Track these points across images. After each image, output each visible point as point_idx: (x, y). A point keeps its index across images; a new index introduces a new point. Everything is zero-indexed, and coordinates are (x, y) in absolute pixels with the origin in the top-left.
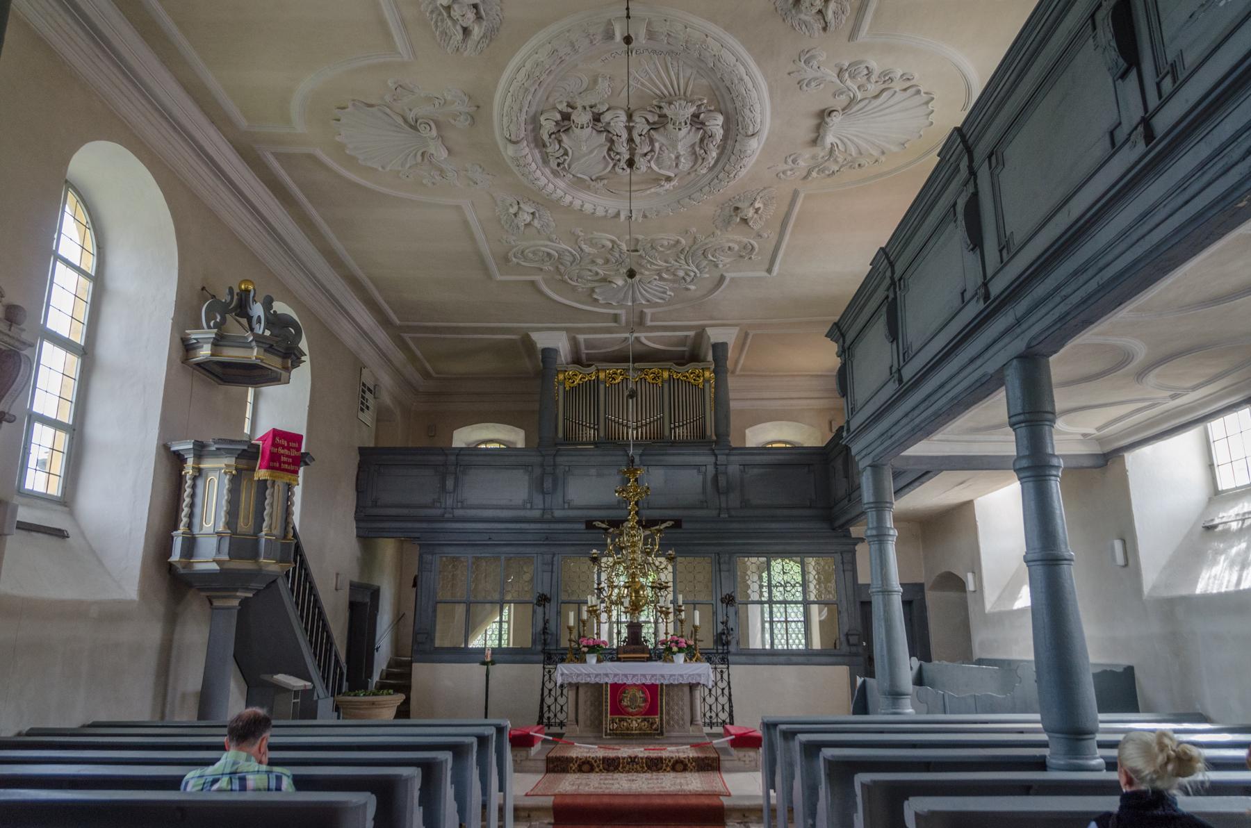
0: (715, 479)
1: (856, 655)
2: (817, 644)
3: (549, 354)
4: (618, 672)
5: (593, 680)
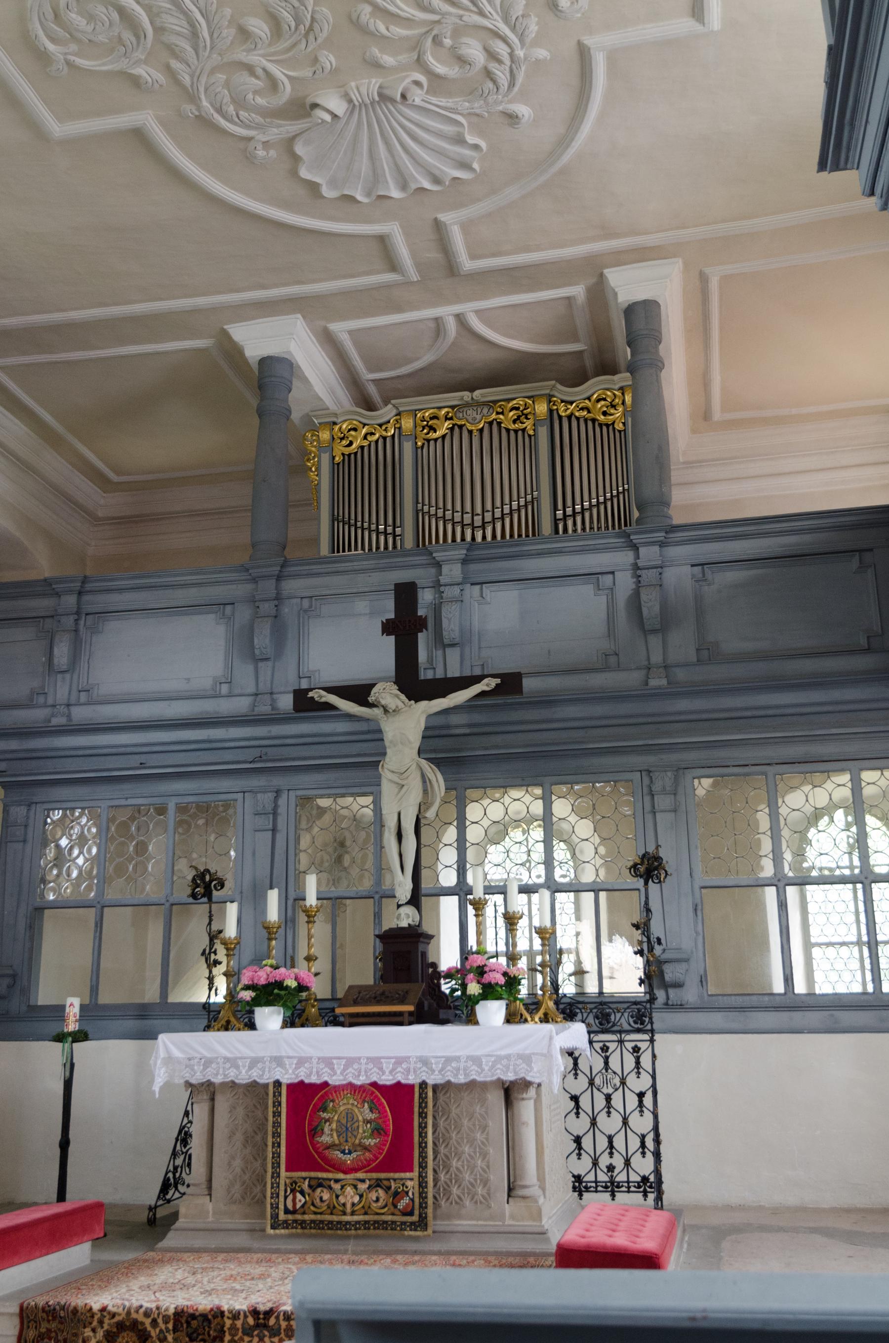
0: (635, 602)
5: (243, 1076)
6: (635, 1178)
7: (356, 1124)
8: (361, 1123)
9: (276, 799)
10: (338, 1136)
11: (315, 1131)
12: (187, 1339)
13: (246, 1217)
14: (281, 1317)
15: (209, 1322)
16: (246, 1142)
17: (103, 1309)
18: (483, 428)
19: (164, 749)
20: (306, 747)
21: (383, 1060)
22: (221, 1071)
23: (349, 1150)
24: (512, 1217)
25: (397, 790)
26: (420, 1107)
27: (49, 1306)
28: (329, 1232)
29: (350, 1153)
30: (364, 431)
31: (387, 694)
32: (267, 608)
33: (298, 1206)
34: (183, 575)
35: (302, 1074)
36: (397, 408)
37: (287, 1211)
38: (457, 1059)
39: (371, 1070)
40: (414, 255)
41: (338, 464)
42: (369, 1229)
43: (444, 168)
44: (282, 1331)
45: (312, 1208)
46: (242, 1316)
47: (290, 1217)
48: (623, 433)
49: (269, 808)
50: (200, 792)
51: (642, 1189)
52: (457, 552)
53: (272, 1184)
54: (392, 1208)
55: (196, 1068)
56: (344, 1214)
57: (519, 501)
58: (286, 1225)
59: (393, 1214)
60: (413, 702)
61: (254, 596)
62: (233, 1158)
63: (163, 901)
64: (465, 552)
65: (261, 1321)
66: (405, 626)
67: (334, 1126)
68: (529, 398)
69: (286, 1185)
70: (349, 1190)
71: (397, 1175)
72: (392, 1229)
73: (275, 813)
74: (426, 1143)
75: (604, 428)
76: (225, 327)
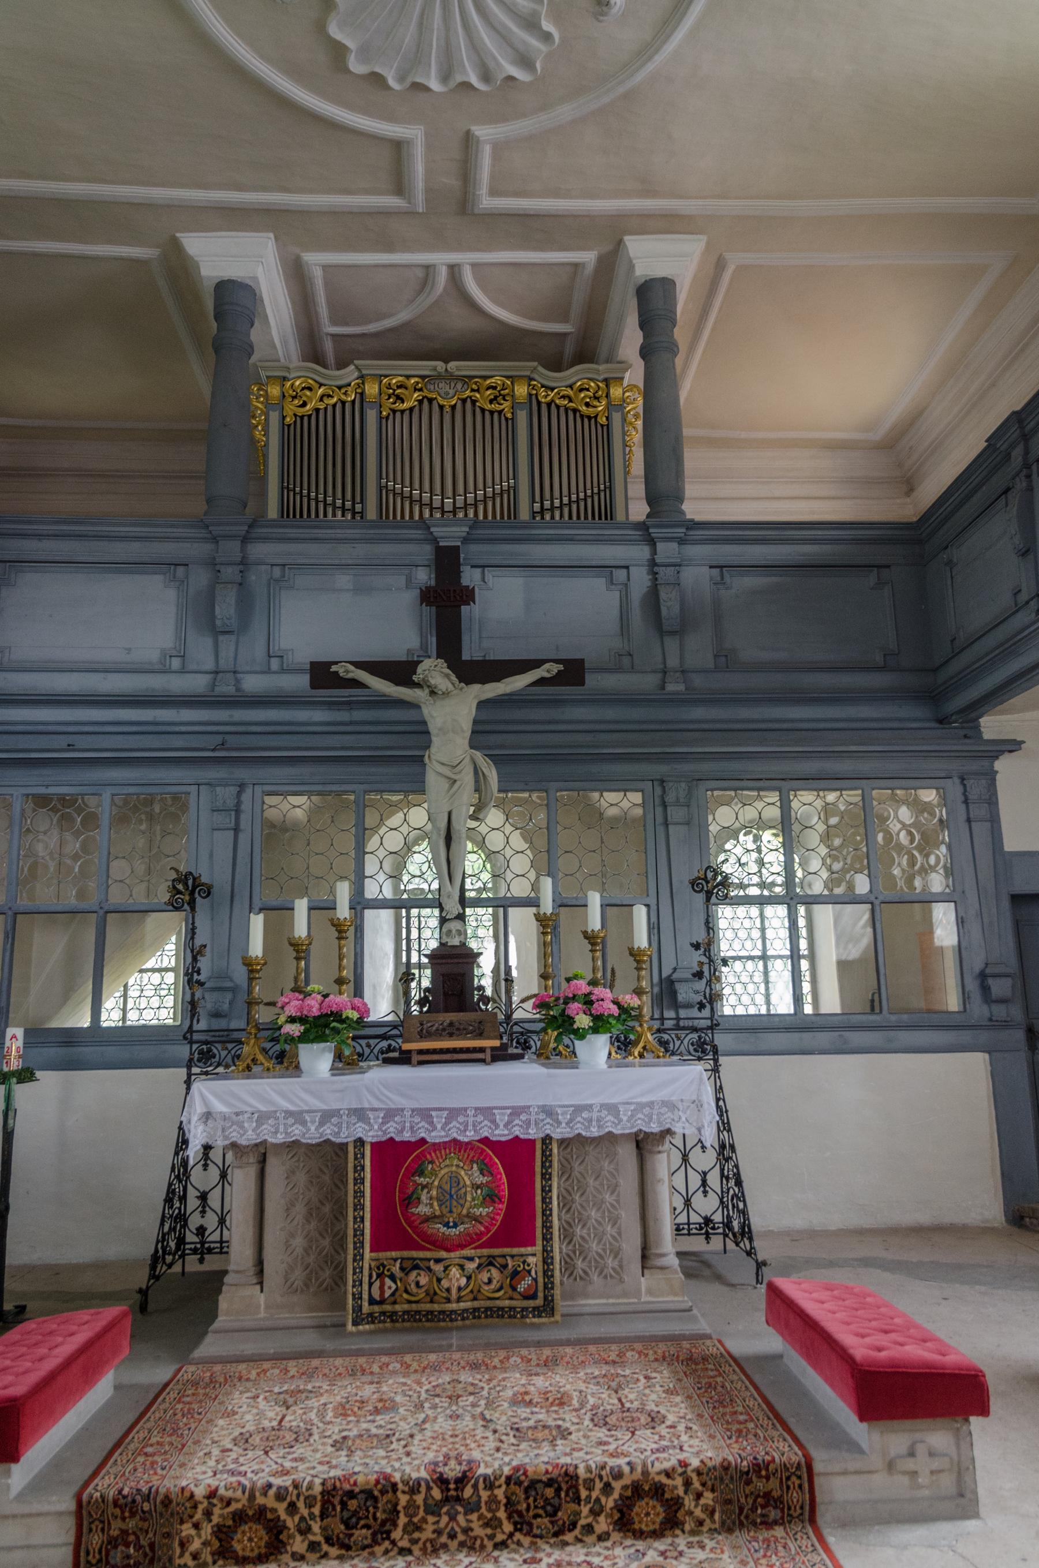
1: (1006, 1025)
2: (831, 1003)
3: (233, 301)
4: (398, 1101)
5: (312, 1134)
6: (695, 1218)
7: (463, 1190)
8: (469, 1189)
9: (239, 794)
10: (440, 1206)
11: (410, 1200)
12: (342, 1527)
13: (311, 1309)
14: (481, 1485)
15: (376, 1499)
16: (308, 1217)
17: (212, 1494)
18: (455, 404)
19: (99, 729)
20: (274, 736)
21: (495, 1111)
22: (281, 1128)
23: (454, 1222)
24: (650, 1292)
25: (447, 786)
26: (543, 1166)
27: (125, 1497)
28: (428, 1324)
29: (455, 1226)
30: (321, 391)
31: (434, 671)
32: (229, 572)
33: (387, 1294)
34: (125, 525)
35: (392, 1129)
36: (360, 370)
37: (372, 1301)
38: (589, 1107)
39: (481, 1123)
40: (429, 172)
41: (289, 426)
42: (479, 1317)
43: (499, 58)
44: (483, 1505)
45: (405, 1296)
46: (423, 1489)
47: (376, 1308)
48: (605, 428)
49: (231, 803)
50: (142, 782)
51: (703, 1231)
52: (458, 529)
53: (354, 1269)
54: (510, 1292)
55: (246, 1125)
56: (448, 1300)
57: (485, 491)
58: (371, 1318)
59: (511, 1298)
60: (463, 684)
61: (214, 558)
62: (292, 1235)
63: (94, 909)
64: (467, 529)
65: (452, 1493)
66: (446, 600)
67: (434, 1193)
68: (507, 377)
69: (370, 1268)
70: (454, 1271)
71: (515, 1251)
72: (510, 1317)
73: (238, 811)
74: (551, 1210)
75: (586, 420)
76: (178, 235)
